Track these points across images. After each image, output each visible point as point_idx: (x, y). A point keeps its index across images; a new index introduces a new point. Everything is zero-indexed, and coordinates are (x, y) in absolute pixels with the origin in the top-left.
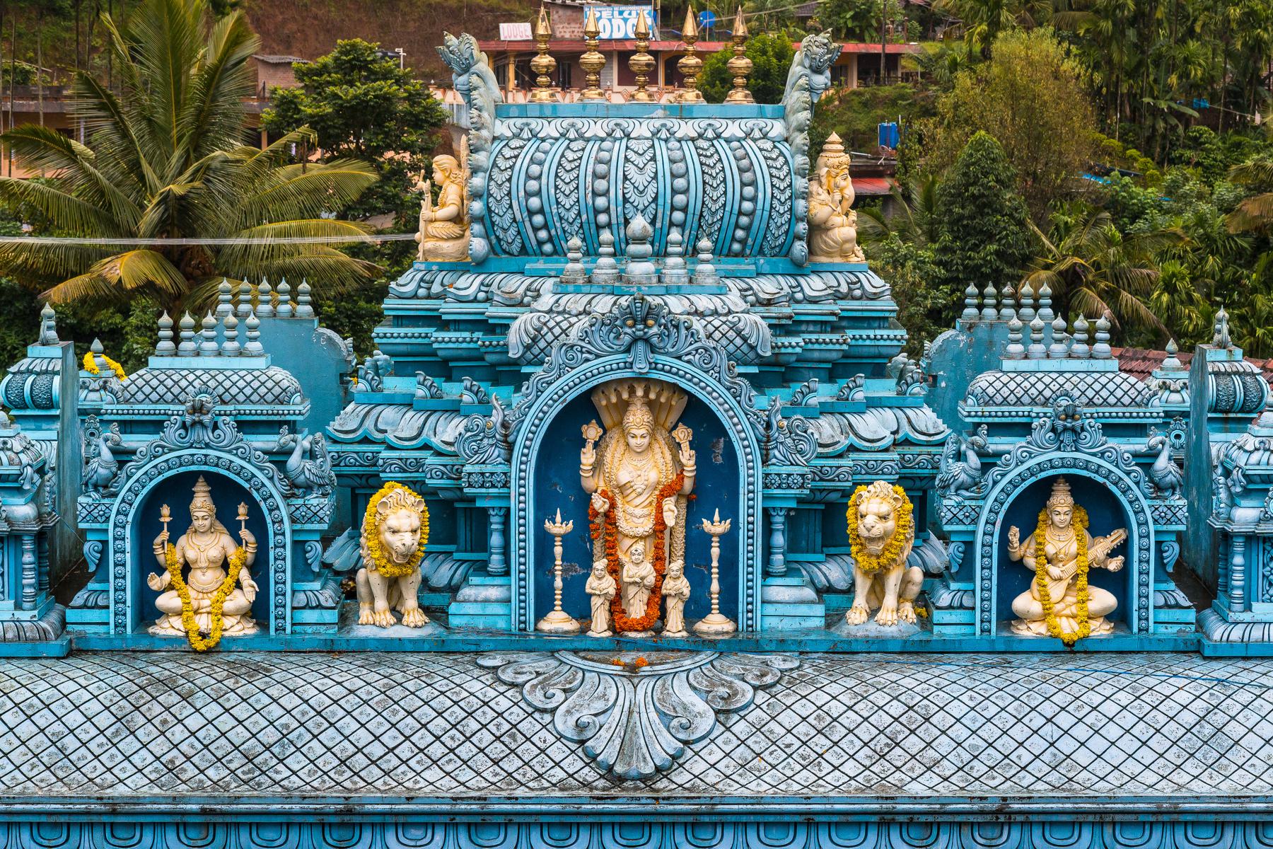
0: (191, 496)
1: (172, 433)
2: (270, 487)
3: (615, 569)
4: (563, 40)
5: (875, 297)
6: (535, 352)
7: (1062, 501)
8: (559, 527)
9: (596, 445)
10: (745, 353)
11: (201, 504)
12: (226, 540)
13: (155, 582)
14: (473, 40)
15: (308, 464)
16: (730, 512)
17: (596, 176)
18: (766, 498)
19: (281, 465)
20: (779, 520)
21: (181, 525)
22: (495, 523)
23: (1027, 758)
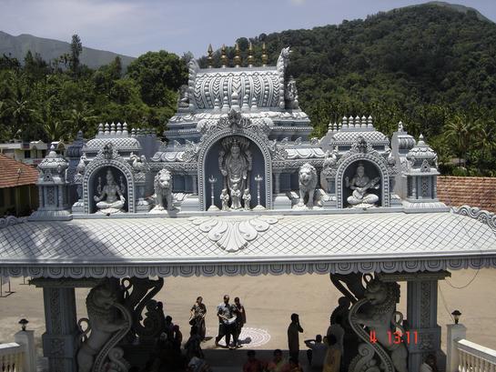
0: (107, 174)
1: (100, 156)
2: (127, 171)
3: (229, 192)
4: (45, 267)
5: (303, 118)
6: (204, 130)
7: (361, 170)
8: (212, 181)
9: (224, 157)
10: (266, 128)
11: (109, 177)
12: (117, 187)
13: (97, 199)
14: (75, 204)
15: (139, 163)
16: (263, 175)
17: (206, 91)
18: (273, 170)
19: (131, 164)
20: (277, 177)
21: (104, 183)
22: (194, 179)
23: (297, 244)
